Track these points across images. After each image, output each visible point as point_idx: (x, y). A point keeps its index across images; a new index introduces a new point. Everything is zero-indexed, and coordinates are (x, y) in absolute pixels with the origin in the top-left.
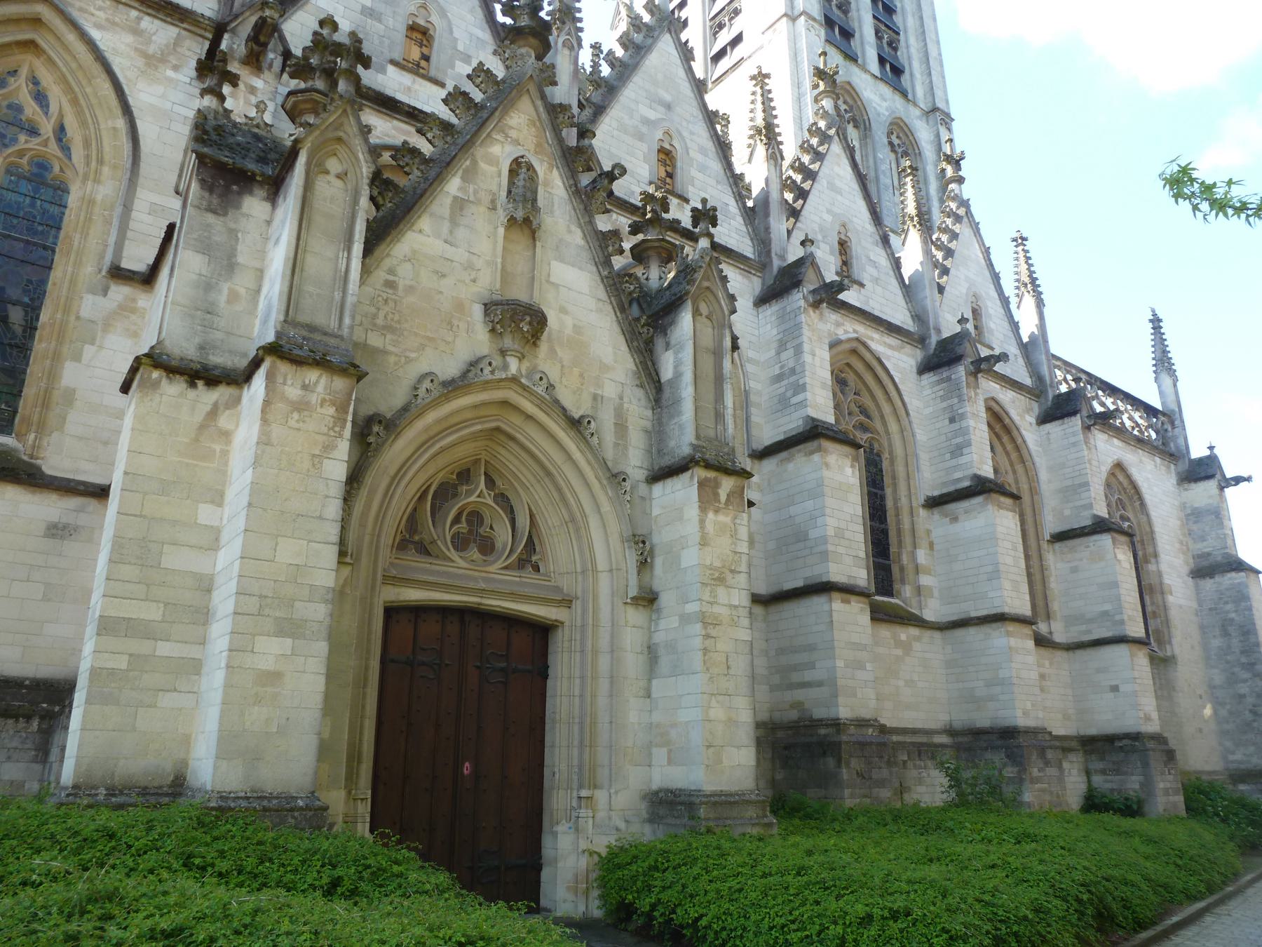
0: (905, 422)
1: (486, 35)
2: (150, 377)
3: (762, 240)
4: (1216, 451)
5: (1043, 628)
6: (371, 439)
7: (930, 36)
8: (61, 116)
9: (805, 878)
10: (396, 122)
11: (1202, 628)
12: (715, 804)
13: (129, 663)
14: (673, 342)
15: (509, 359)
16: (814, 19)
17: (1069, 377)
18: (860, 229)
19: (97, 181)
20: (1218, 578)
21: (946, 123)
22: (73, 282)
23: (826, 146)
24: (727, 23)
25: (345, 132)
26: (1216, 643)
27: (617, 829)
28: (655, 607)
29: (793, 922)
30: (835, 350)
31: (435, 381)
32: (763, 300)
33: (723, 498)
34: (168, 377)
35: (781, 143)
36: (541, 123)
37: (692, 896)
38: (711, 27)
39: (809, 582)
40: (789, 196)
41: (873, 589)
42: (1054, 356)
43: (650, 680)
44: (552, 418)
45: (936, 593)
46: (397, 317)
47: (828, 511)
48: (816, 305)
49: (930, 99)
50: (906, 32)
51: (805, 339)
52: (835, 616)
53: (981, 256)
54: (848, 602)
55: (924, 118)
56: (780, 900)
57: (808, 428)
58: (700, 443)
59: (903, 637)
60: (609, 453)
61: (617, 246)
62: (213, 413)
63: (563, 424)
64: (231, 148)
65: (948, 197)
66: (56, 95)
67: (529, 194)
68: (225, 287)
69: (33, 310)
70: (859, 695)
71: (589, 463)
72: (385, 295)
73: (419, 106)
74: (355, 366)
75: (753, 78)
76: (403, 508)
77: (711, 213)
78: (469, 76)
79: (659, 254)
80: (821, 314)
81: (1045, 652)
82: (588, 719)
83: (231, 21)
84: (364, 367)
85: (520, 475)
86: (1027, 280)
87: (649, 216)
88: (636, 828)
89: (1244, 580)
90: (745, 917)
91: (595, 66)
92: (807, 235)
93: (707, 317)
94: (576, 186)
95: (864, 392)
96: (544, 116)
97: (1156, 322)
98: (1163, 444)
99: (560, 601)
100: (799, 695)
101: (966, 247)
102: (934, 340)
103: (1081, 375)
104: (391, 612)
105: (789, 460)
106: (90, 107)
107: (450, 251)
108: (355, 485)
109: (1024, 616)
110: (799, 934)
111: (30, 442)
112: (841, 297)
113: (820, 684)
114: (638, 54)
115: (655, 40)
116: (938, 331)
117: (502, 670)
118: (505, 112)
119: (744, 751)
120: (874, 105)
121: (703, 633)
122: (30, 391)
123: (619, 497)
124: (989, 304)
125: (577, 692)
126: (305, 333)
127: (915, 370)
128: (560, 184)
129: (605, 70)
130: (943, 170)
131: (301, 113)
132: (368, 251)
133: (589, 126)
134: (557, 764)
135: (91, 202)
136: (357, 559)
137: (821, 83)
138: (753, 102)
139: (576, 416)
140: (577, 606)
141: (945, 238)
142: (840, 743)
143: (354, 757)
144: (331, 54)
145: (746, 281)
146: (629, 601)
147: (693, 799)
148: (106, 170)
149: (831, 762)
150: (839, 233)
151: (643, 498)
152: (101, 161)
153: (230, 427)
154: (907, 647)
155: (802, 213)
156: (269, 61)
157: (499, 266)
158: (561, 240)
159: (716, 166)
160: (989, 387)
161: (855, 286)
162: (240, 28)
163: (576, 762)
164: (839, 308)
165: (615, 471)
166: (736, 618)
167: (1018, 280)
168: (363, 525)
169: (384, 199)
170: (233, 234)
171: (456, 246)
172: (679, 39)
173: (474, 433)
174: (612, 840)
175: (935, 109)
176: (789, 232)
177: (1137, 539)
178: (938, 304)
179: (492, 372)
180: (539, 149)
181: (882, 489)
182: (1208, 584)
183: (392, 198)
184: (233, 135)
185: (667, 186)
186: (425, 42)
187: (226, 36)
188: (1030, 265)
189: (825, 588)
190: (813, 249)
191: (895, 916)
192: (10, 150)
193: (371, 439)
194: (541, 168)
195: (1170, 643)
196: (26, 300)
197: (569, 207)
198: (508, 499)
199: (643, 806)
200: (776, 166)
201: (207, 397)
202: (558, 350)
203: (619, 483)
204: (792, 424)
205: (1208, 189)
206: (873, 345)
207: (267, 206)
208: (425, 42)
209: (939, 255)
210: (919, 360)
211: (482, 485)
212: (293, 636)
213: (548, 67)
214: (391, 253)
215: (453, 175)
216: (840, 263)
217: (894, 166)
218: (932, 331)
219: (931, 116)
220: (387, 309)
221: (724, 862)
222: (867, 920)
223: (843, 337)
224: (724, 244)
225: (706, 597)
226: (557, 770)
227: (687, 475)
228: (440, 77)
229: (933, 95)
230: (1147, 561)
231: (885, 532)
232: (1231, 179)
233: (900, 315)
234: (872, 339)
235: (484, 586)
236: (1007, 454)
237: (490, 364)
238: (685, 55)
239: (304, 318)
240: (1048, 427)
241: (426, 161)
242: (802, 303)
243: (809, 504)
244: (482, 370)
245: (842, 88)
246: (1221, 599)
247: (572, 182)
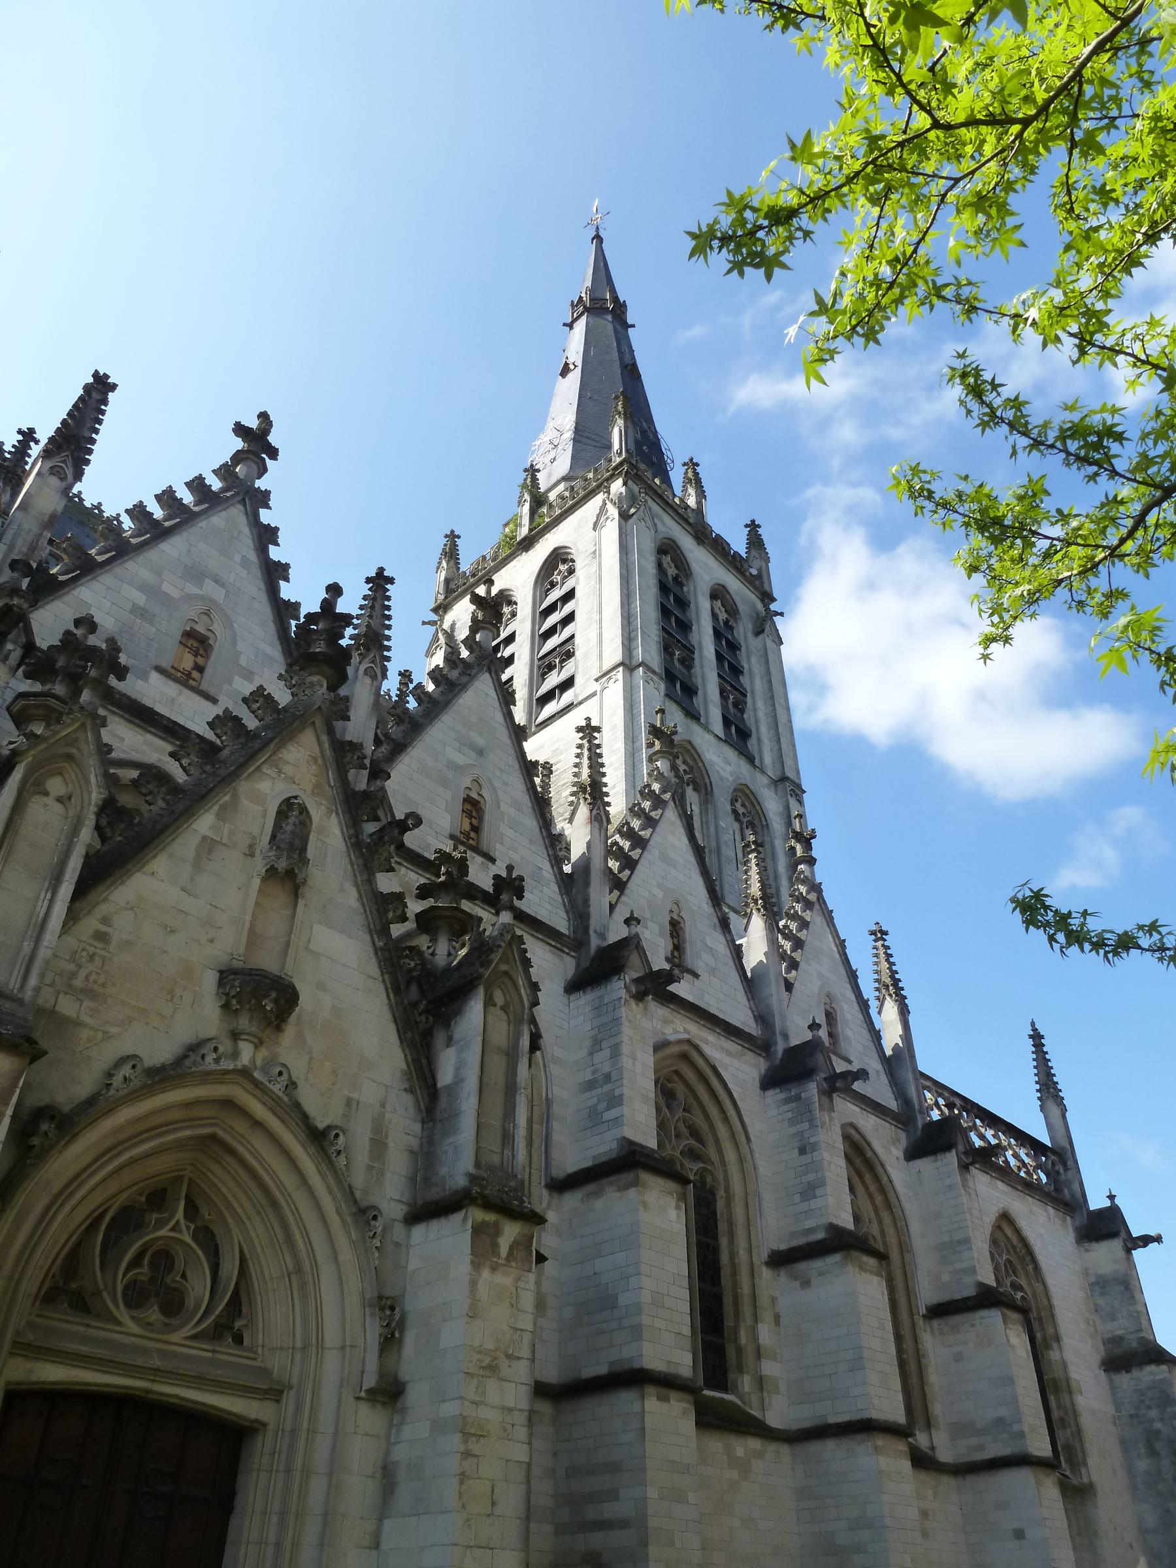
0: (745, 1150)
1: (274, 651)
3: (579, 912)
4: (1117, 1201)
5: (921, 1439)
7: (779, 701)
10: (149, 737)
11: (1123, 1442)
14: (456, 1037)
15: (242, 1044)
16: (654, 672)
17: (941, 1101)
18: (696, 908)
20: (1136, 1373)
21: (797, 795)
23: (660, 811)
25: (78, 749)
26: (1142, 1465)
28: (399, 1405)
30: (661, 1054)
31: (139, 1068)
32: (575, 986)
33: (504, 1250)
35: (609, 804)
36: (324, 761)
38: (539, 667)
40: (614, 865)
41: (701, 1381)
42: (922, 1074)
43: (380, 1520)
44: (288, 1127)
45: (783, 1387)
46: (102, 979)
48: (639, 997)
49: (779, 767)
50: (753, 694)
51: (625, 1039)
53: (835, 949)
54: (666, 1399)
55: (772, 788)
58: (481, 1173)
59: (740, 1452)
60: (358, 1178)
61: (399, 912)
63: (302, 1135)
65: (798, 879)
72: (91, 950)
73: (181, 721)
74: (32, 1042)
75: (580, 729)
76: (62, 1241)
77: (517, 883)
78: (245, 700)
80: (646, 1008)
81: (927, 1478)
84: (43, 1043)
85: (236, 1205)
86: (888, 981)
87: (443, 878)
89: (1167, 1375)
91: (402, 695)
92: (632, 912)
93: (503, 1008)
94: (357, 837)
96: (328, 753)
97: (1037, 1038)
98: (1056, 1189)
99: (266, 1392)
100: (596, 1540)
101: (817, 938)
102: (780, 1047)
103: (954, 1099)
105: (597, 1194)
109: (894, 1423)
112: (671, 988)
113: (624, 1524)
115: (472, 678)
116: (786, 1037)
118: (282, 745)
121: (462, 1448)
124: (845, 1006)
125: (272, 1537)
127: (757, 1084)
129: (412, 704)
130: (793, 849)
131: (30, 719)
132: (80, 893)
133: (384, 766)
137: (657, 742)
138: (578, 756)
139: (321, 1124)
140: (289, 1399)
141: (793, 926)
144: (80, 659)
146: (363, 1394)
150: (671, 911)
151: (397, 1244)
154: (744, 1467)
155: (629, 885)
156: (5, 651)
157: (247, 925)
159: (530, 823)
160: (846, 1109)
161: (687, 976)
165: (364, 1204)
166: (509, 1428)
167: (877, 981)
171: (196, 897)
172: (499, 679)
173: (180, 1140)
175: (784, 779)
176: (612, 907)
177: (1033, 1315)
178: (786, 1004)
179: (217, 1061)
180: (317, 790)
181: (715, 1237)
182: (1124, 1380)
185: (471, 842)
186: (201, 652)
188: (892, 964)
190: (638, 929)
193: (35, 1141)
194: (317, 812)
195: (1085, 1465)
197: (345, 862)
198: (213, 1236)
203: (368, 1222)
204: (603, 1146)
205: (1063, 919)
206: (708, 1050)
208: (201, 652)
209: (787, 945)
210: (763, 1071)
211: (180, 1214)
213: (341, 699)
214: (111, 898)
215: (206, 811)
216: (670, 947)
217: (738, 837)
218: (779, 1038)
219: (780, 786)
220: (91, 967)
223: (672, 1038)
224: (533, 914)
228: (212, 692)
229: (783, 764)
230: (1048, 1347)
231: (718, 1299)
232: (1086, 910)
233: (740, 1015)
234: (707, 1042)
235: (157, 1362)
236: (870, 1196)
237: (216, 1049)
238: (504, 697)
240: (919, 1163)
242: (623, 993)
244: (203, 1057)
245: (681, 746)
246: (1142, 1401)
247: (352, 832)
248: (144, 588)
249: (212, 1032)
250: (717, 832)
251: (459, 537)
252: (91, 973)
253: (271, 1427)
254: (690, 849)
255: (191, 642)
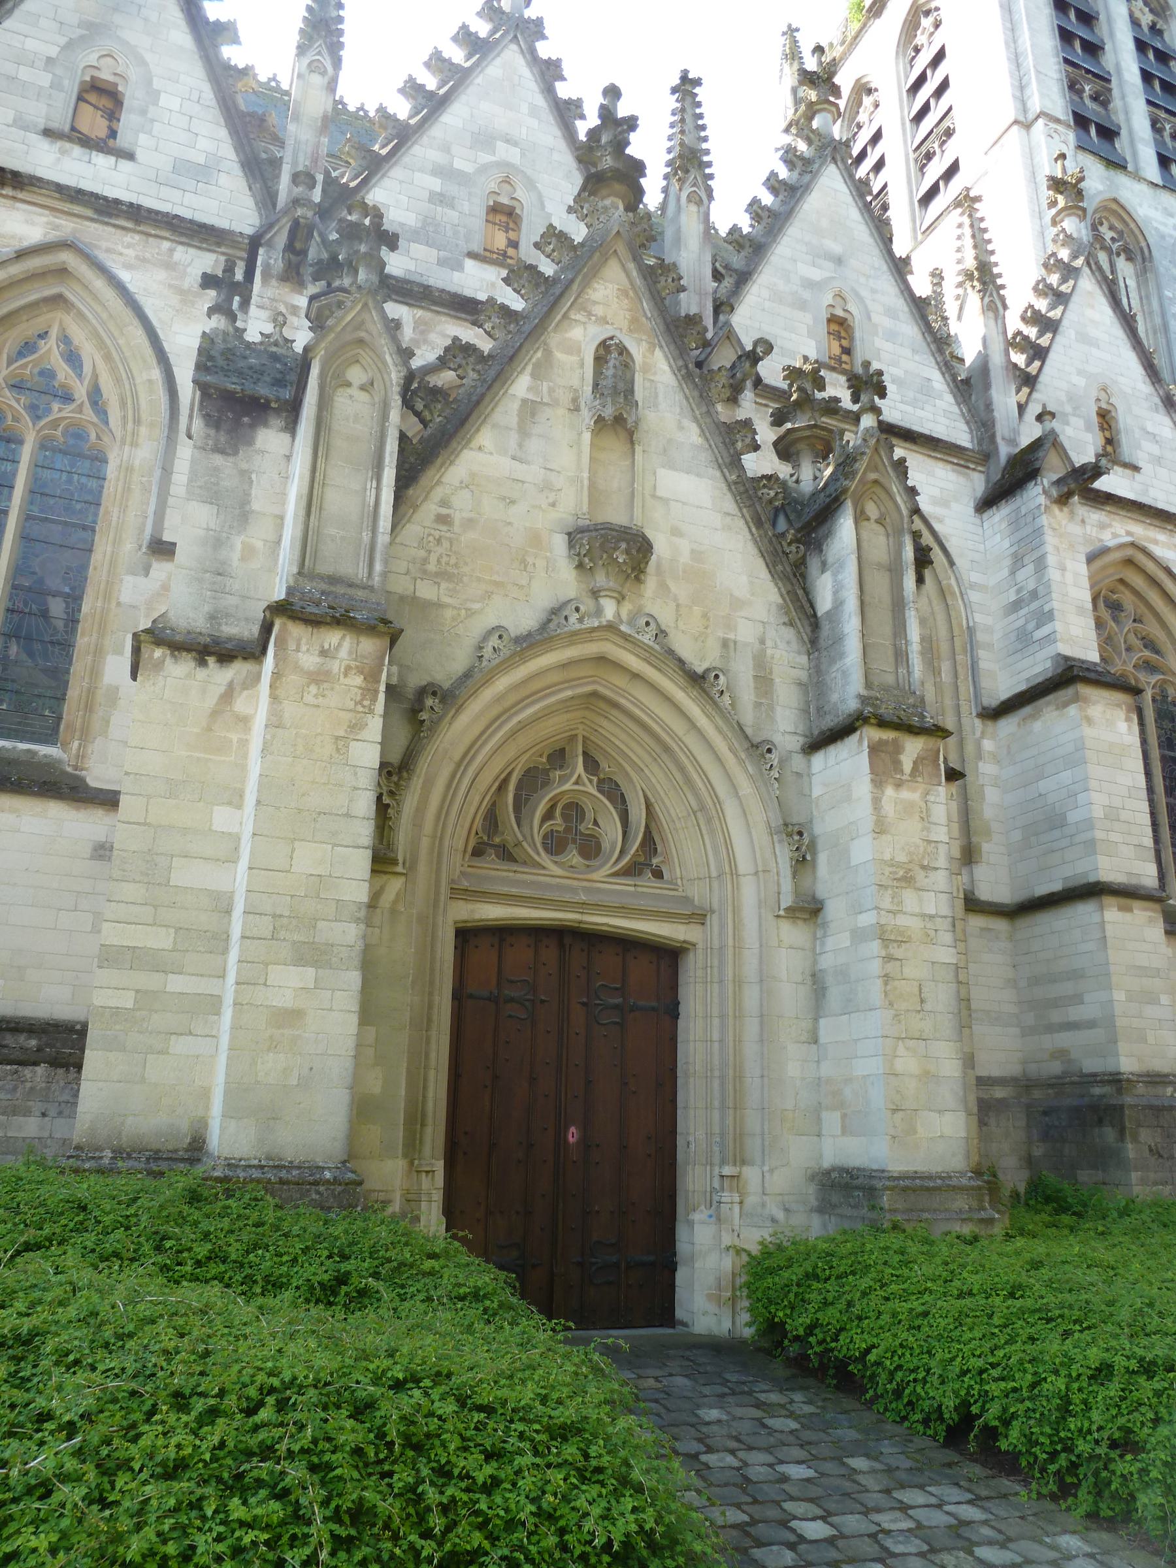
2: (151, 657)
6: (424, 716)
8: (95, 376)
9: (1019, 1303)
12: (905, 1189)
13: (136, 1002)
14: (830, 560)
15: (602, 601)
16: (1057, 121)
18: (1129, 391)
19: (134, 444)
22: (113, 563)
23: (1071, 282)
24: (938, 151)
27: (774, 1220)
28: (819, 921)
29: (994, 1366)
30: (1098, 564)
32: (987, 503)
33: (907, 766)
34: (173, 655)
35: (1003, 287)
37: (860, 1318)
38: (916, 161)
39: (1071, 884)
40: (1019, 359)
43: (816, 1020)
46: (453, 561)
47: (1093, 784)
48: (1063, 500)
51: (1049, 548)
52: (1110, 931)
54: (1129, 910)
56: (978, 1335)
57: (1059, 671)
58: (873, 693)
60: (748, 716)
61: (748, 440)
62: (228, 695)
64: (240, 374)
66: (88, 351)
67: (621, 386)
68: (238, 542)
69: (74, 599)
70: (1151, 1040)
71: (720, 731)
74: (386, 622)
79: (812, 447)
80: (1072, 513)
82: (731, 1072)
83: (265, 232)
84: (397, 624)
87: (795, 397)
88: (798, 1220)
90: (929, 1352)
92: (1044, 406)
93: (877, 522)
95: (1149, 617)
96: (638, 282)
100: (1064, 1039)
104: (466, 936)
105: (1034, 717)
106: (124, 360)
107: (520, 470)
108: (405, 774)
110: (1003, 1385)
111: (74, 751)
113: (1091, 1024)
114: (792, 197)
115: (815, 175)
117: (616, 1007)
118: (586, 285)
119: (948, 1117)
120: (1155, 224)
121: (883, 953)
122: (74, 693)
123: (762, 774)
125: (716, 1036)
126: (324, 586)
128: (667, 368)
134: (692, 1130)
135: (129, 469)
136: (412, 866)
139: (700, 670)
140: (714, 921)
142: (1122, 1107)
143: (415, 1119)
145: (962, 480)
146: (782, 913)
147: (875, 1182)
148: (143, 430)
149: (1109, 1134)
150: (1098, 400)
151: (799, 775)
152: (137, 421)
153: (250, 711)
157: (586, 482)
158: (670, 441)
162: (277, 239)
163: (717, 1130)
164: (1103, 504)
165: (756, 740)
166: (932, 933)
168: (418, 823)
169: (431, 413)
170: (245, 475)
171: (527, 463)
174: (766, 1234)
176: (1021, 408)
179: (581, 620)
180: (634, 325)
183: (442, 411)
184: (245, 358)
186: (511, 225)
187: (261, 251)
189: (1093, 891)
190: (1055, 424)
191: (1148, 1369)
192: (42, 423)
193: (424, 716)
194: (638, 350)
196: (67, 590)
197: (679, 397)
199: (812, 1189)
200: (996, 319)
201: (219, 676)
202: (671, 584)
203: (763, 756)
204: (1038, 667)
206: (1158, 551)
207: (286, 437)
208: (511, 225)
211: (580, 769)
212: (316, 964)
216: (1101, 441)
221: (906, 1272)
222: (1103, 1373)
224: (927, 432)
225: (886, 903)
226: (691, 1139)
227: (855, 737)
234: (1156, 542)
237: (577, 610)
239: (324, 568)
241: (483, 359)
242: (1042, 499)
243: (1066, 776)
244: (566, 618)
247: (680, 363)
248: (440, 171)
249: (571, 593)
250: (1161, 305)
251: (797, 30)
252: (441, 555)
253: (700, 946)
254: (1115, 321)
255: (500, 218)
